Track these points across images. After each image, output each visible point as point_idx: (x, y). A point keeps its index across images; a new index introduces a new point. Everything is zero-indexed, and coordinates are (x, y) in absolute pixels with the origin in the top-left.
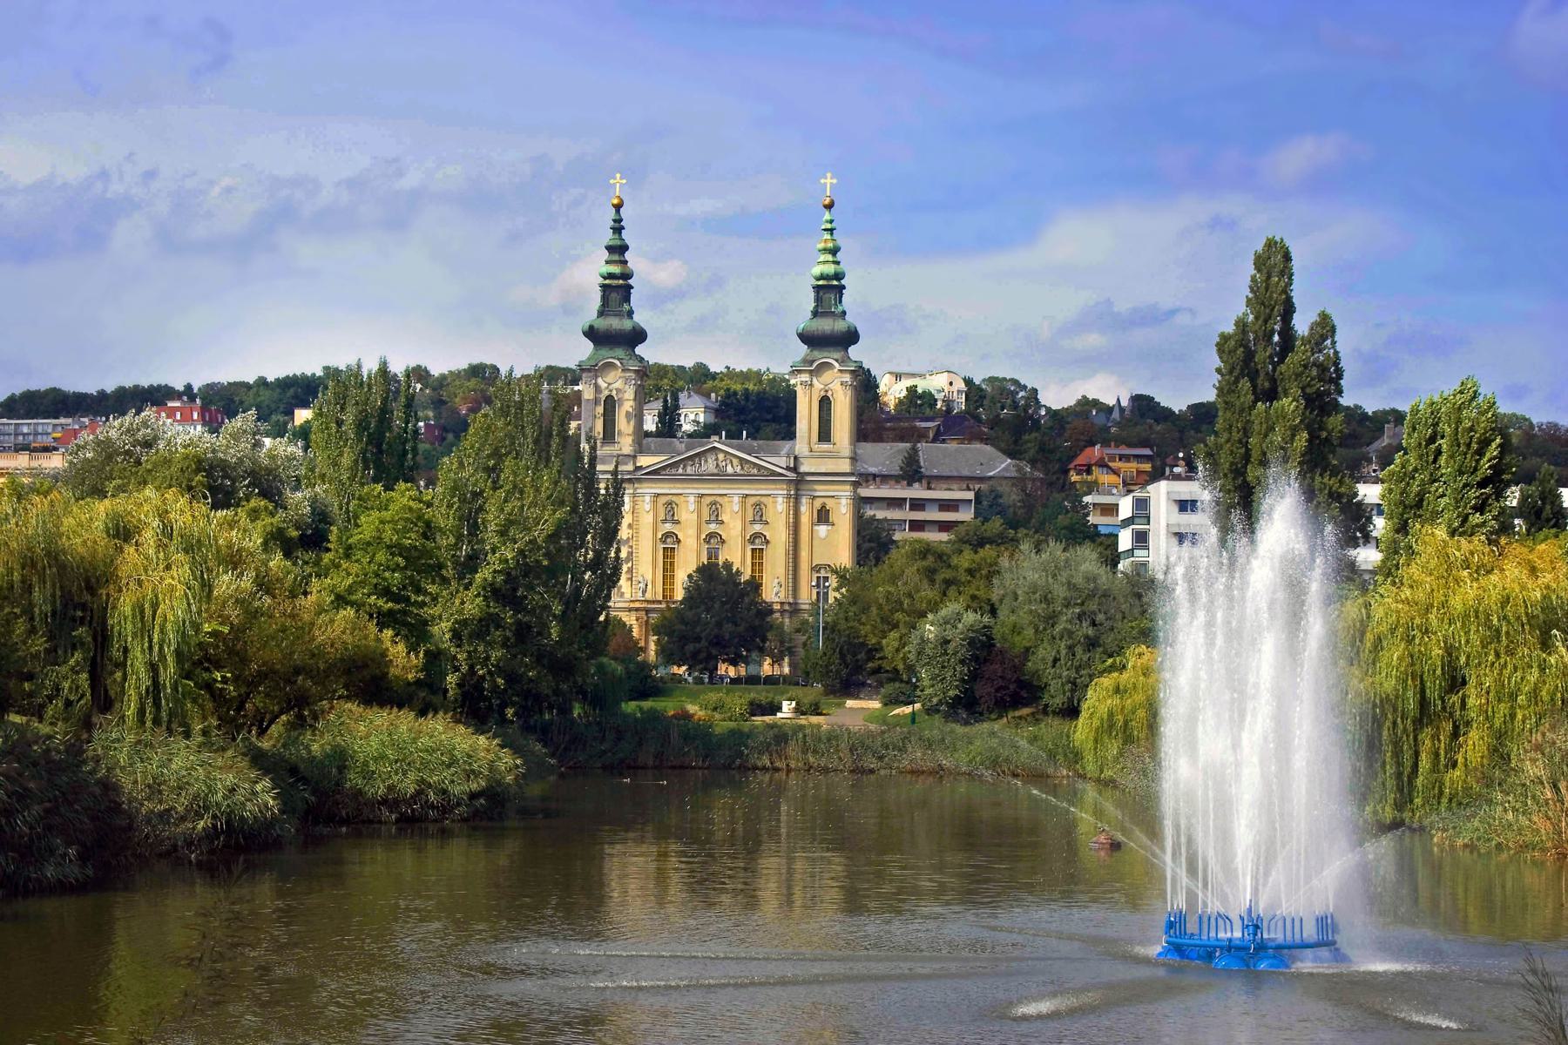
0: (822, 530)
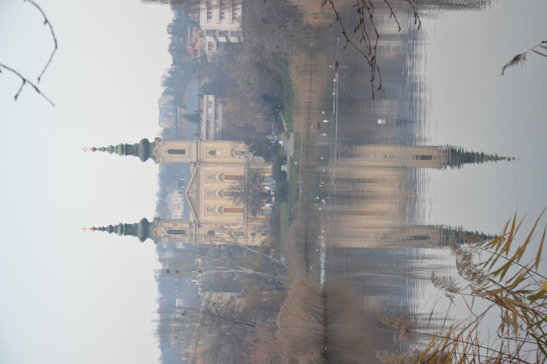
0: (218, 153)
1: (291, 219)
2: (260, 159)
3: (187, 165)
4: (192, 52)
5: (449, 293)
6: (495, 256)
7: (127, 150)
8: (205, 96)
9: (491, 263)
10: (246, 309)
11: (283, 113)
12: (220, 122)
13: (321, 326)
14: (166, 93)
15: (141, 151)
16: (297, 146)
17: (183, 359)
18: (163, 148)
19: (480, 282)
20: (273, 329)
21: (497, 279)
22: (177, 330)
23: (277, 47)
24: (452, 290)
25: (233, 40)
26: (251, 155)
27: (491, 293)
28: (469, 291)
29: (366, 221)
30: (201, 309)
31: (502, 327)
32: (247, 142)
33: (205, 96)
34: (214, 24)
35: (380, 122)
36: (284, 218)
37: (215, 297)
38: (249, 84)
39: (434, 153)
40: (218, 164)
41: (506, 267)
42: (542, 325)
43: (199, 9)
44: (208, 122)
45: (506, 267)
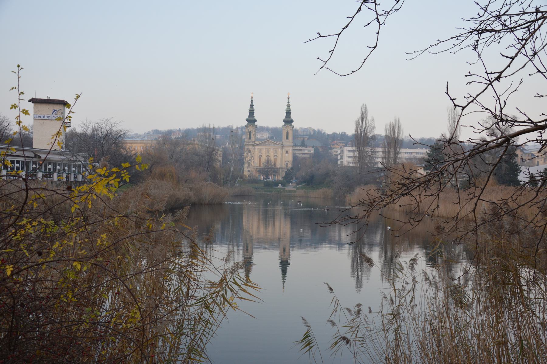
0: (287, 155)
1: (256, 188)
2: (284, 174)
3: (281, 140)
4: (333, 143)
5: (225, 259)
6: (242, 280)
7: (288, 113)
8: (313, 149)
9: (239, 278)
10: (214, 167)
11: (306, 185)
12: (301, 156)
13: (207, 202)
14: (314, 131)
15: (288, 119)
16: (290, 191)
17: (192, 139)
18: (289, 129)
19: (231, 272)
20: (205, 180)
21: (232, 280)
22: (205, 136)
23: (336, 182)
24: (227, 260)
25: (339, 162)
26: (286, 170)
27: (225, 279)
28: (226, 268)
29: (255, 224)
30: (215, 147)
31: (210, 282)
32: (292, 168)
33: (313, 149)
34: (346, 153)
35: (301, 229)
36: (257, 185)
37: (220, 153)
38: (319, 169)
39: (286, 254)
40: (282, 155)
41: (236, 283)
42: (211, 299)
43: (353, 146)
44: (301, 150)
45: (236, 283)
